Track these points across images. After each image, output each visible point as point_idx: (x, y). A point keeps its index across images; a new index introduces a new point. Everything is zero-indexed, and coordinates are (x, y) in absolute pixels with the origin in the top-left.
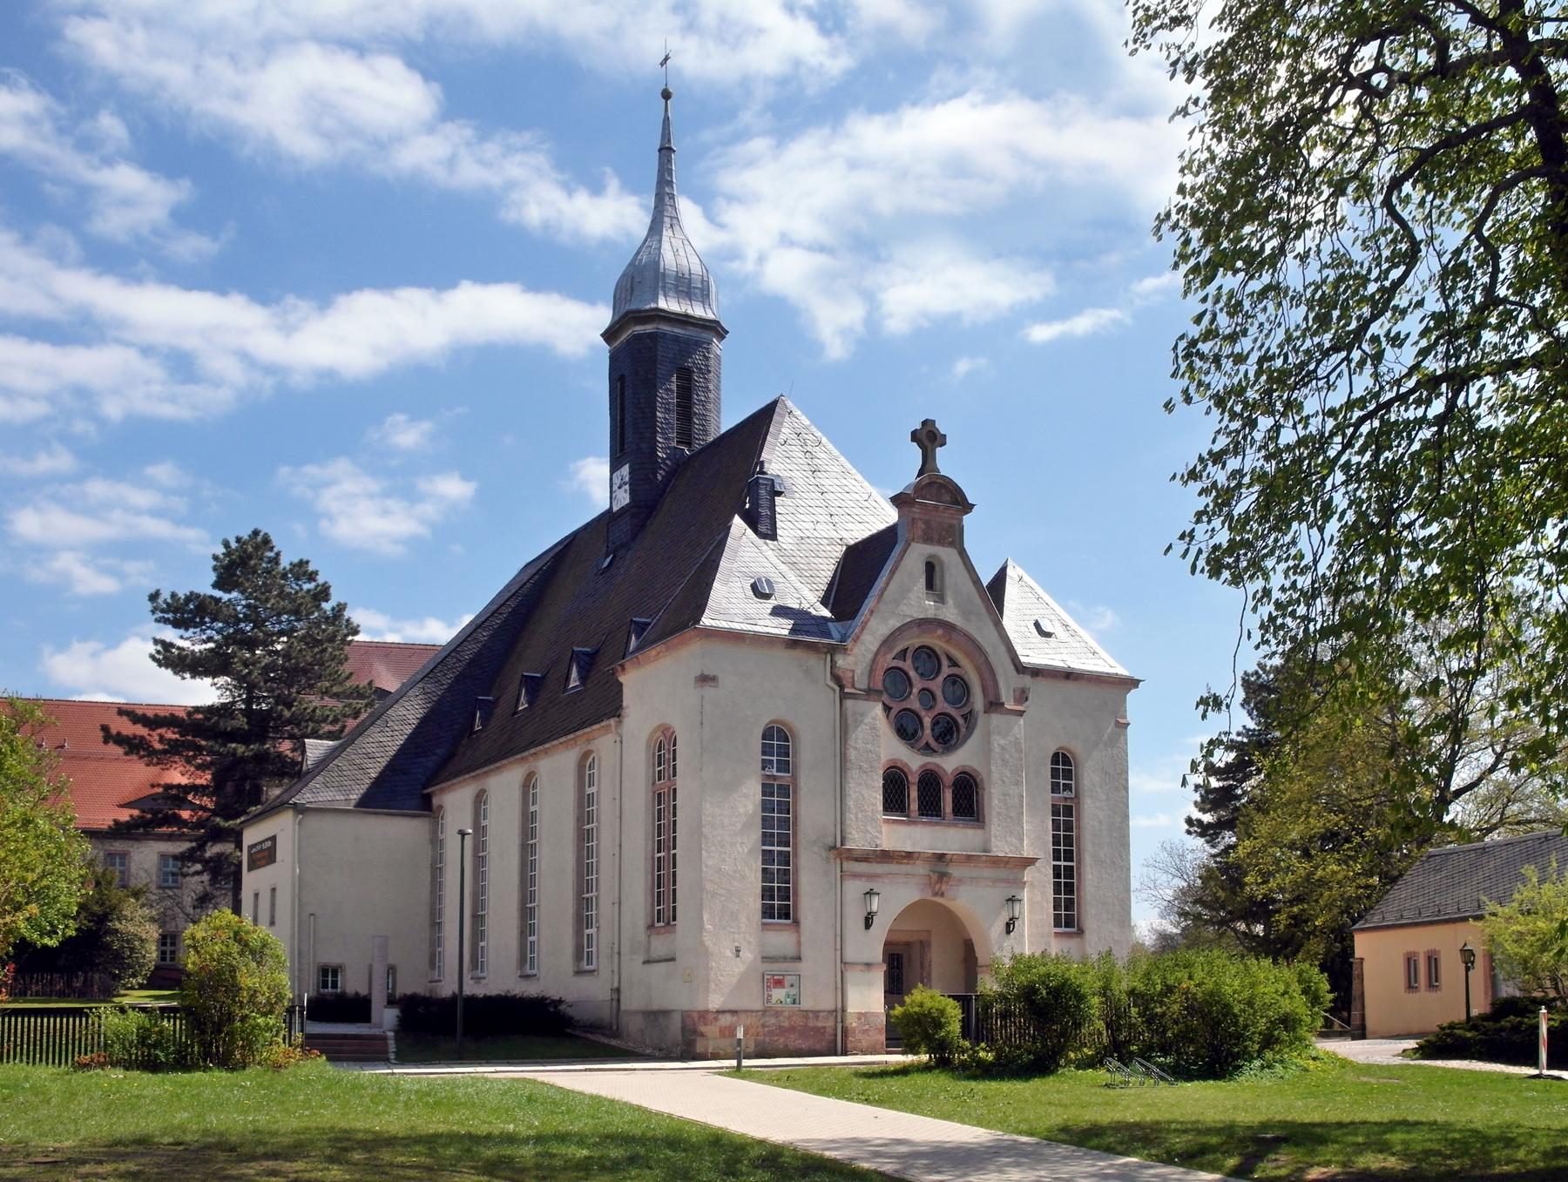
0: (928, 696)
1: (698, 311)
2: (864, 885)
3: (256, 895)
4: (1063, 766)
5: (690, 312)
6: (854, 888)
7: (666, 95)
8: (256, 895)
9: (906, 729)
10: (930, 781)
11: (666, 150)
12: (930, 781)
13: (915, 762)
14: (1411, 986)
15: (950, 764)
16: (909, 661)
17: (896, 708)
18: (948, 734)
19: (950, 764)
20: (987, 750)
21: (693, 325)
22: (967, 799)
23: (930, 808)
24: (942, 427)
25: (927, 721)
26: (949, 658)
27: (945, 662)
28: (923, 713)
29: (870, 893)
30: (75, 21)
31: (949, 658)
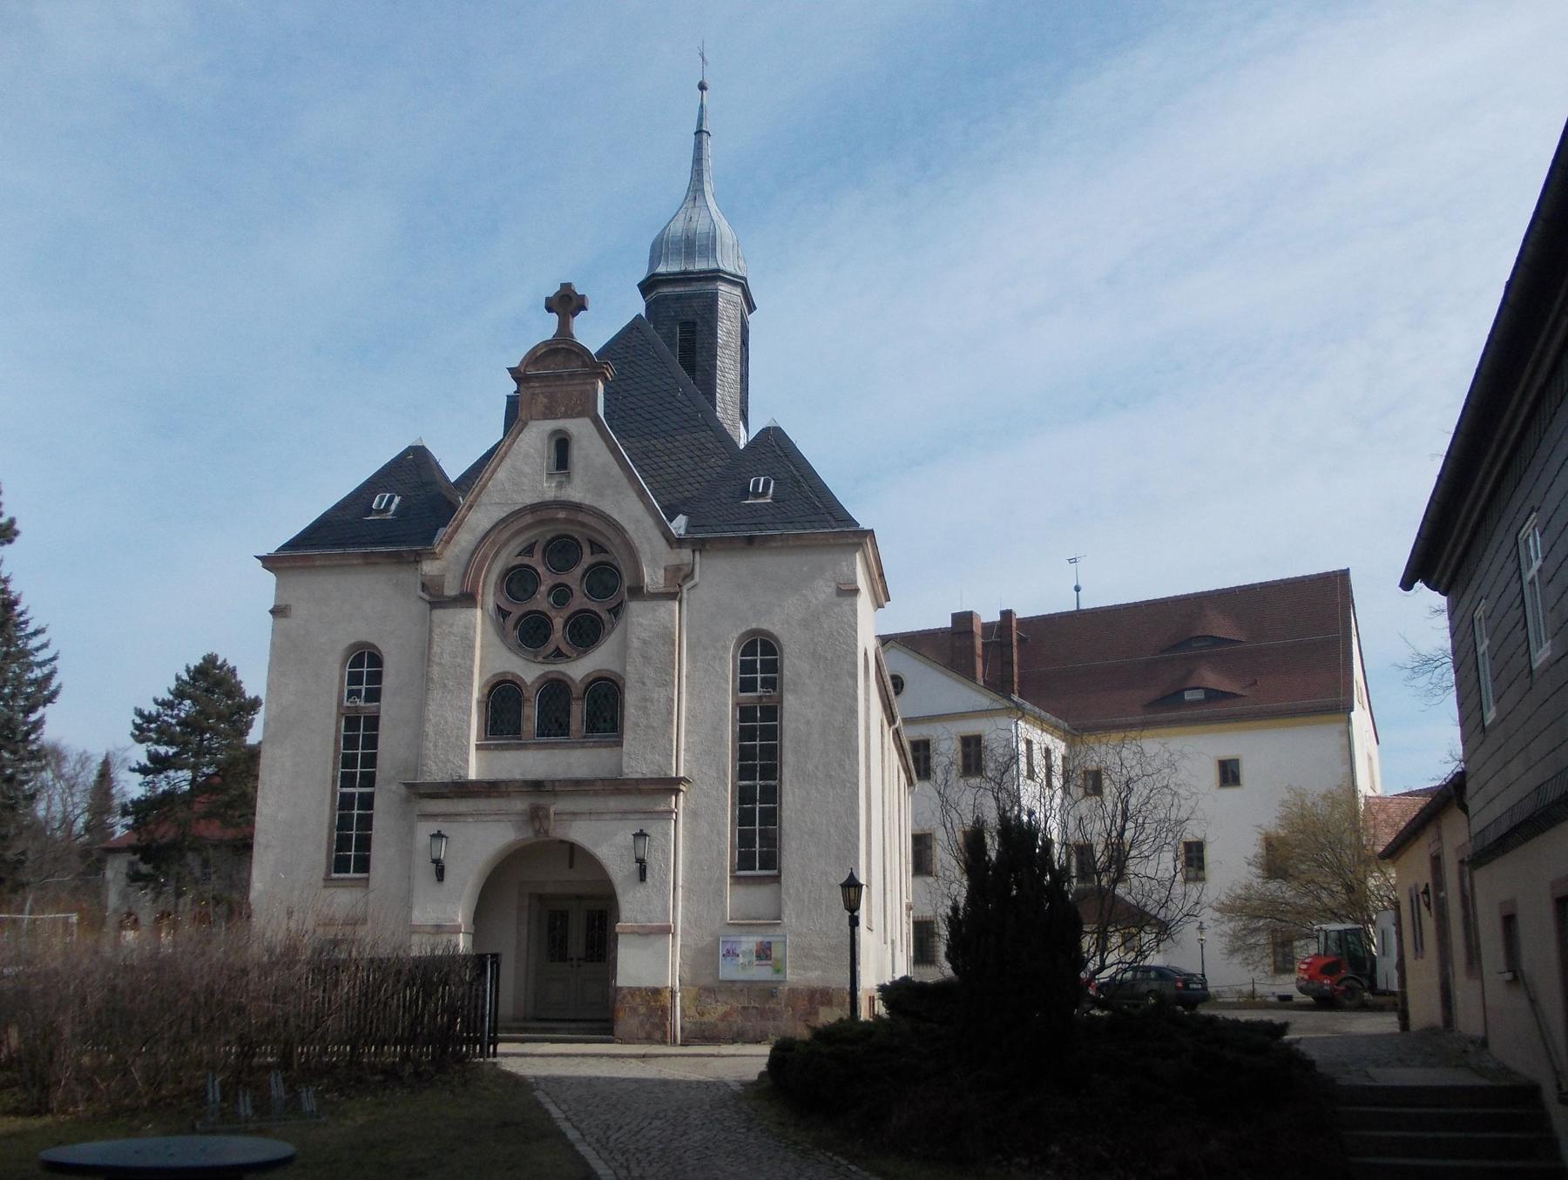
0: (561, 594)
1: (700, 265)
2: (433, 827)
3: (1509, 921)
4: (760, 658)
5: (690, 268)
6: (424, 830)
7: (702, 87)
8: (1509, 921)
9: (530, 633)
10: (555, 691)
11: (699, 132)
12: (555, 691)
13: (529, 672)
14: (495, 956)
15: (579, 670)
16: (538, 555)
17: (517, 611)
18: (586, 632)
19: (579, 670)
20: (624, 645)
21: (699, 279)
22: (604, 708)
23: (554, 727)
24: (553, 290)
25: (558, 622)
26: (592, 543)
27: (586, 550)
28: (552, 614)
29: (439, 836)
30: (694, 225)
31: (592, 543)
